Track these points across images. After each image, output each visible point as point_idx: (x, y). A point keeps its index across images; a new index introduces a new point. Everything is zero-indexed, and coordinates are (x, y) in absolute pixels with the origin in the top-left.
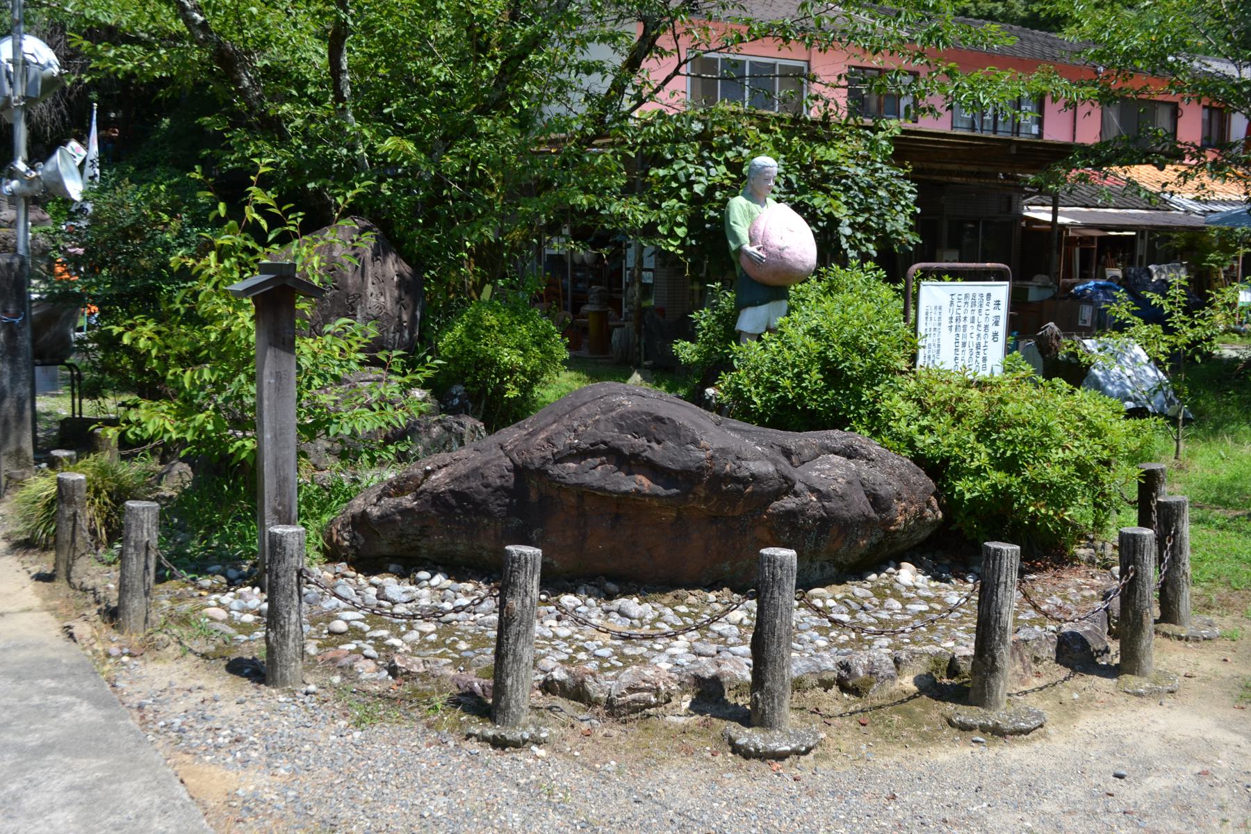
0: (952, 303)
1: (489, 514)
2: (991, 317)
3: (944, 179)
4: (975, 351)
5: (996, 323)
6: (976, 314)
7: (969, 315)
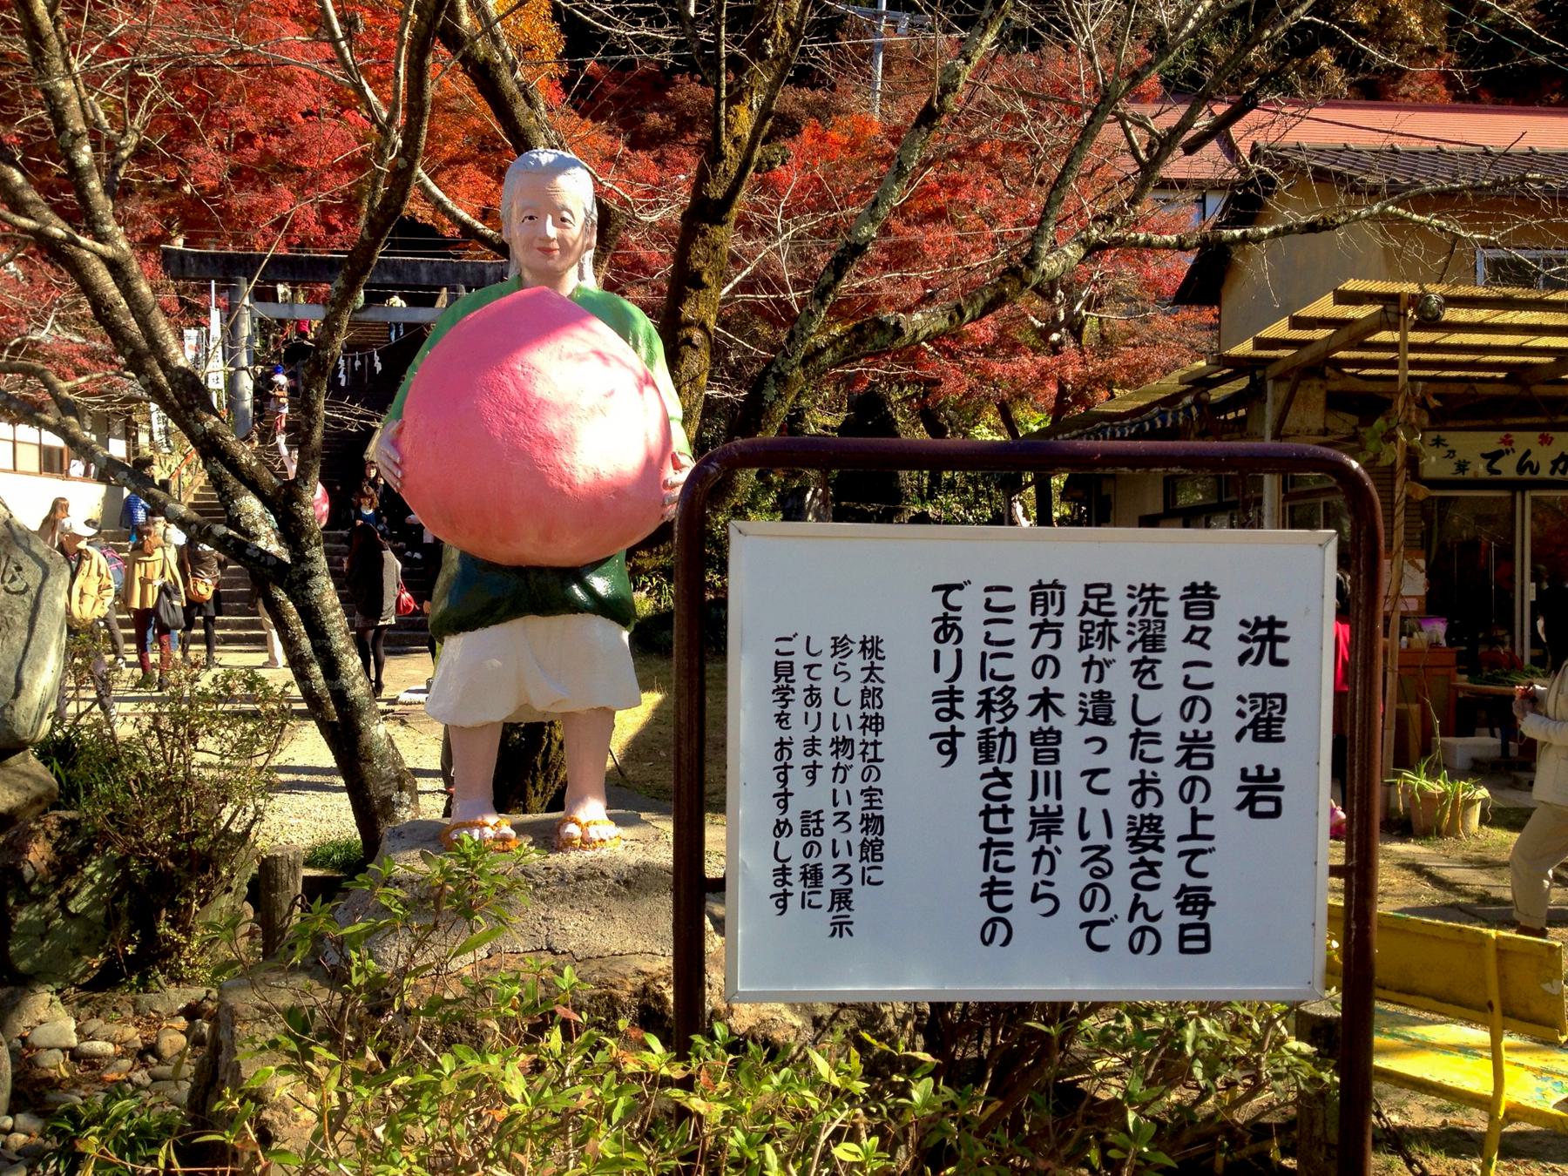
0: (947, 627)
1: (894, 339)
2: (1224, 702)
3: (1273, 353)
4: (1121, 856)
6: (1120, 682)
7: (1071, 685)
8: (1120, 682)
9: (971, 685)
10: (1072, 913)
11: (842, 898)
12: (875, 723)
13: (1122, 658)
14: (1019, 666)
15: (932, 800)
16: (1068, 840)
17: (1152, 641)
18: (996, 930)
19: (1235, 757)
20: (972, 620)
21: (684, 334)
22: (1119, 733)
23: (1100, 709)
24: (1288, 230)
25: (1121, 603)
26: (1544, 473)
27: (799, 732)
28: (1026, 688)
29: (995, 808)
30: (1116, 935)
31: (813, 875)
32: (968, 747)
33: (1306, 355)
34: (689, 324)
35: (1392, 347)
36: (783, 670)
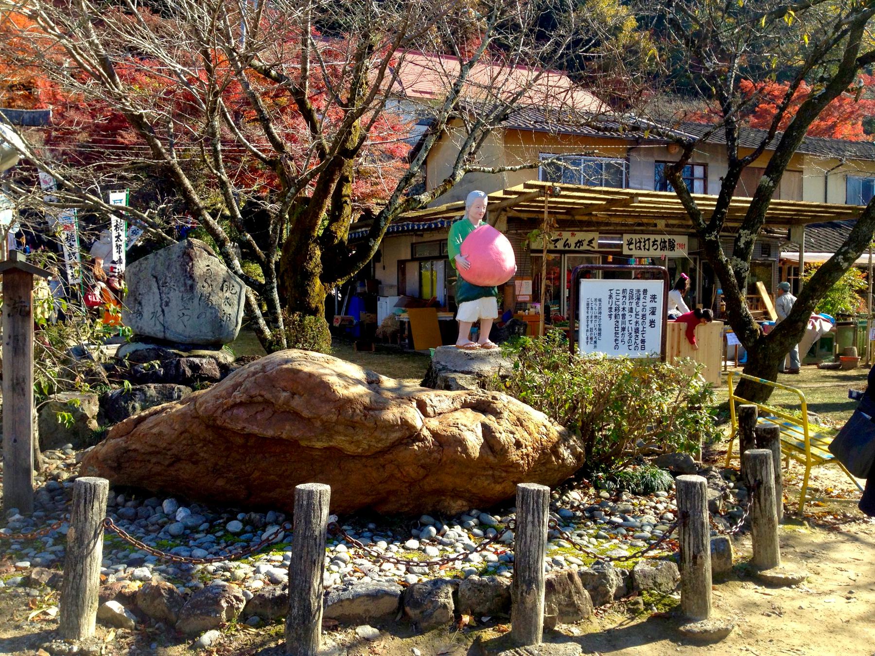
0: (611, 297)
2: (648, 308)
4: (633, 334)
5: (653, 313)
6: (634, 306)
7: (627, 306)
8: (634, 306)
9: (614, 306)
10: (627, 344)
11: (595, 342)
12: (600, 313)
13: (634, 301)
14: (620, 303)
15: (608, 325)
16: (626, 332)
17: (639, 299)
18: (616, 347)
19: (649, 317)
20: (614, 296)
21: (344, 199)
22: (633, 314)
23: (631, 310)
24: (524, 167)
25: (635, 292)
26: (572, 248)
27: (590, 315)
28: (621, 307)
29: (617, 327)
30: (632, 347)
31: (591, 338)
32: (613, 317)
33: (505, 203)
34: (345, 196)
35: (543, 202)
36: (588, 304)
